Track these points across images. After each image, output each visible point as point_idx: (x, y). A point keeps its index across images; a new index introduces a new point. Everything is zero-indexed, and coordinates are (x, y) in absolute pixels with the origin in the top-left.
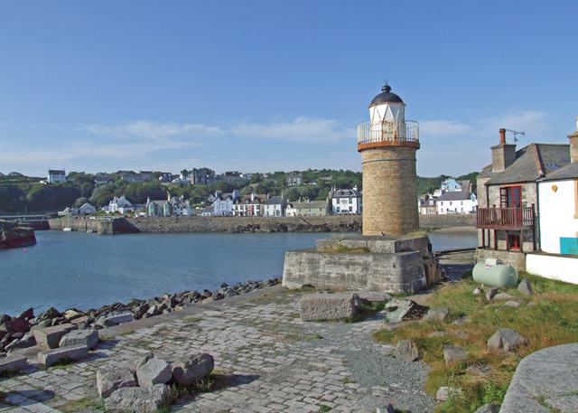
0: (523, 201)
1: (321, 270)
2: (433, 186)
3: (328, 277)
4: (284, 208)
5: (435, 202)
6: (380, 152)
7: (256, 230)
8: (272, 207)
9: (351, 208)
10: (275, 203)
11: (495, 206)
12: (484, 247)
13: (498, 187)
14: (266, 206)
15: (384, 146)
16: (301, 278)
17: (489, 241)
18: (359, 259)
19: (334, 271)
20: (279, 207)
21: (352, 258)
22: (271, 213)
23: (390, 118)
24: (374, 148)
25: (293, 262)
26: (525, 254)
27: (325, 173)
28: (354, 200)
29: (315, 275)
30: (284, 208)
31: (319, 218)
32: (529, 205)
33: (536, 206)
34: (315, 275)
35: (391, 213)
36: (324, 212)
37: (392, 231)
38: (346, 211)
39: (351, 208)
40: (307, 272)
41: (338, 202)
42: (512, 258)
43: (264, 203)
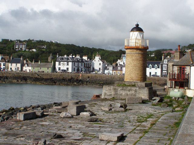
0: (140, 48)
1: (118, 92)
2: (115, 58)
3: (121, 95)
4: (22, 66)
5: (121, 68)
6: (135, 50)
7: (5, 80)
8: (14, 65)
9: (68, 68)
10: (17, 62)
11: (175, 73)
12: (171, 87)
13: (177, 67)
14: (10, 64)
15: (137, 49)
16: (110, 95)
17: (172, 85)
18: (134, 88)
19: (124, 93)
20: (19, 65)
21: (131, 88)
22: (13, 69)
23: (139, 37)
24: (133, 49)
25: (107, 89)
26: (185, 90)
27: (41, 43)
28: (70, 64)
29: (116, 94)
30: (22, 66)
31: (48, 74)
32: (187, 74)
33: (189, 75)
34: (116, 94)
35: (138, 74)
36: (50, 70)
37: (137, 80)
38: (65, 71)
39: (68, 68)
40: (113, 93)
41: (59, 64)
42: (182, 90)
43: (8, 62)
